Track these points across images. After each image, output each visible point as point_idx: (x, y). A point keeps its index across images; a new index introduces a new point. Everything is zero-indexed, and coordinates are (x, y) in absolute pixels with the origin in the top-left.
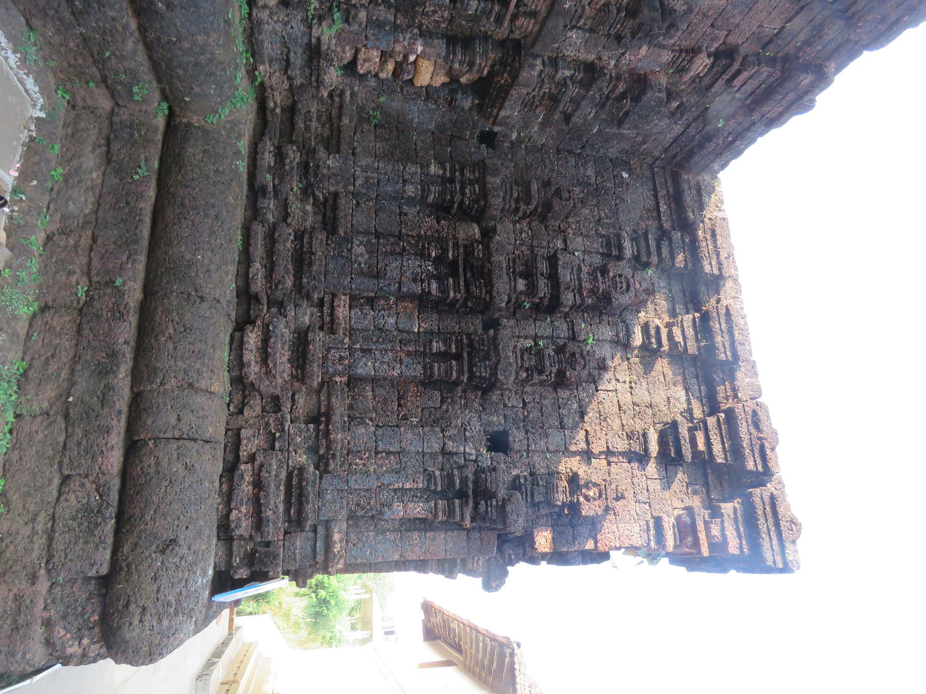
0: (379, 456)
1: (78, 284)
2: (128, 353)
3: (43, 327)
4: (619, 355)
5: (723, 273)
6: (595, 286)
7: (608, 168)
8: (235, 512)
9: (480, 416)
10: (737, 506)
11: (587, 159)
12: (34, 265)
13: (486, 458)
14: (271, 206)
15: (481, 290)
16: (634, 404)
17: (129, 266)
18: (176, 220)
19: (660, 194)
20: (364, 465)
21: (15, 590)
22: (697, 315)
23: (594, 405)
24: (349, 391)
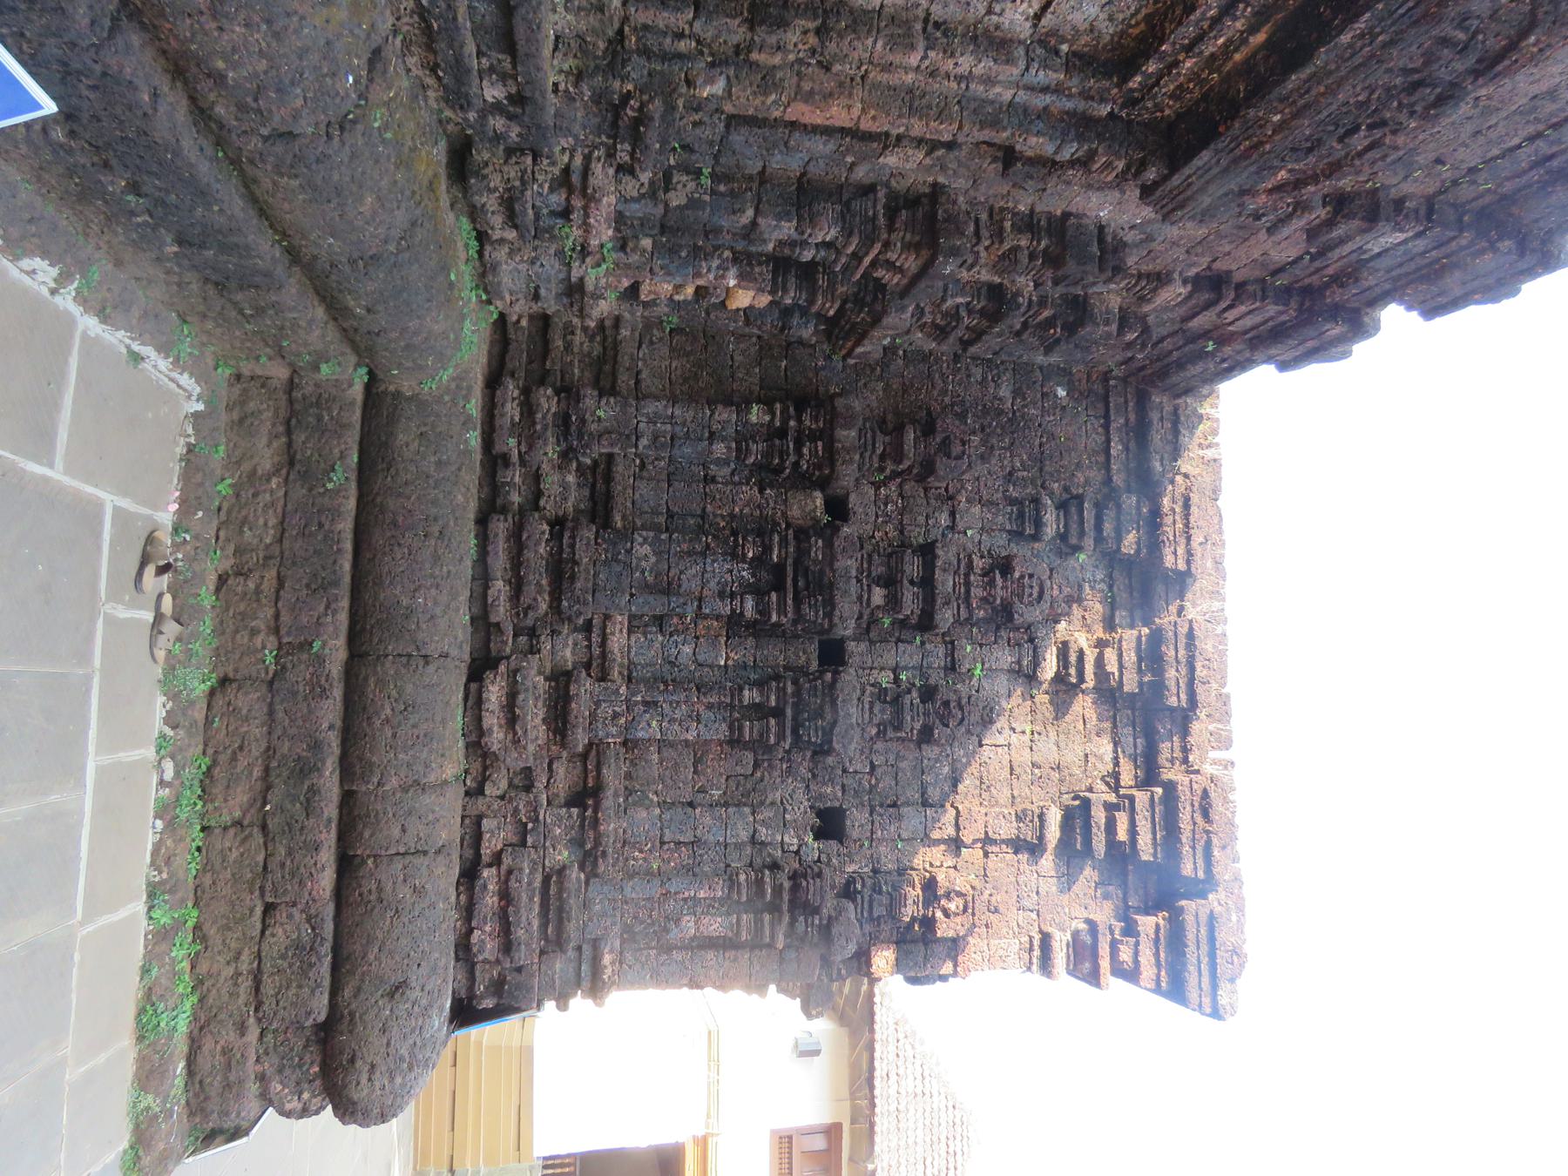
0: (666, 847)
1: (264, 647)
2: (333, 740)
3: (225, 709)
4: (1019, 692)
5: (1193, 569)
6: (989, 594)
7: (1035, 383)
8: (477, 933)
9: (808, 786)
10: (1161, 922)
11: (1001, 368)
12: (207, 626)
13: (813, 846)
14: (517, 479)
15: (817, 612)
16: (1033, 765)
17: (329, 619)
18: (387, 549)
19: (1113, 425)
20: (645, 859)
21: (222, 1042)
22: (1146, 631)
23: (974, 768)
24: (627, 752)
